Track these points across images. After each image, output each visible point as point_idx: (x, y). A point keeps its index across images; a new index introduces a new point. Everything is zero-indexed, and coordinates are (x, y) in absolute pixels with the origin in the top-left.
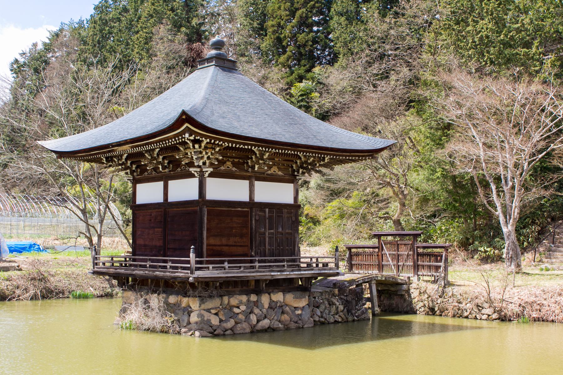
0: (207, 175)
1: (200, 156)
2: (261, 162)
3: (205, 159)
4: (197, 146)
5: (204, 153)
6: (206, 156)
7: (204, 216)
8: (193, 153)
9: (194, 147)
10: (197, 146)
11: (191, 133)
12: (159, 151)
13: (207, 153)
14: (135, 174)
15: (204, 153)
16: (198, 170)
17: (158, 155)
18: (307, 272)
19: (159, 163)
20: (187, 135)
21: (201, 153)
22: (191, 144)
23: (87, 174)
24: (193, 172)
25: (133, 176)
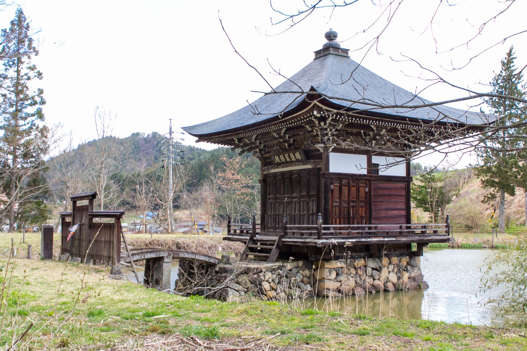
0: (331, 149)
1: (325, 132)
2: (378, 137)
3: (330, 135)
4: (322, 124)
5: (329, 130)
6: (330, 133)
7: (282, 167)
8: (318, 130)
9: (319, 124)
10: (322, 124)
11: (320, 110)
12: (286, 130)
13: (331, 130)
14: (263, 152)
15: (329, 130)
16: (323, 145)
17: (284, 133)
18: (393, 225)
19: (285, 141)
20: (315, 113)
21: (326, 129)
22: (317, 122)
23: (489, 260)
24: (318, 148)
25: (262, 155)
